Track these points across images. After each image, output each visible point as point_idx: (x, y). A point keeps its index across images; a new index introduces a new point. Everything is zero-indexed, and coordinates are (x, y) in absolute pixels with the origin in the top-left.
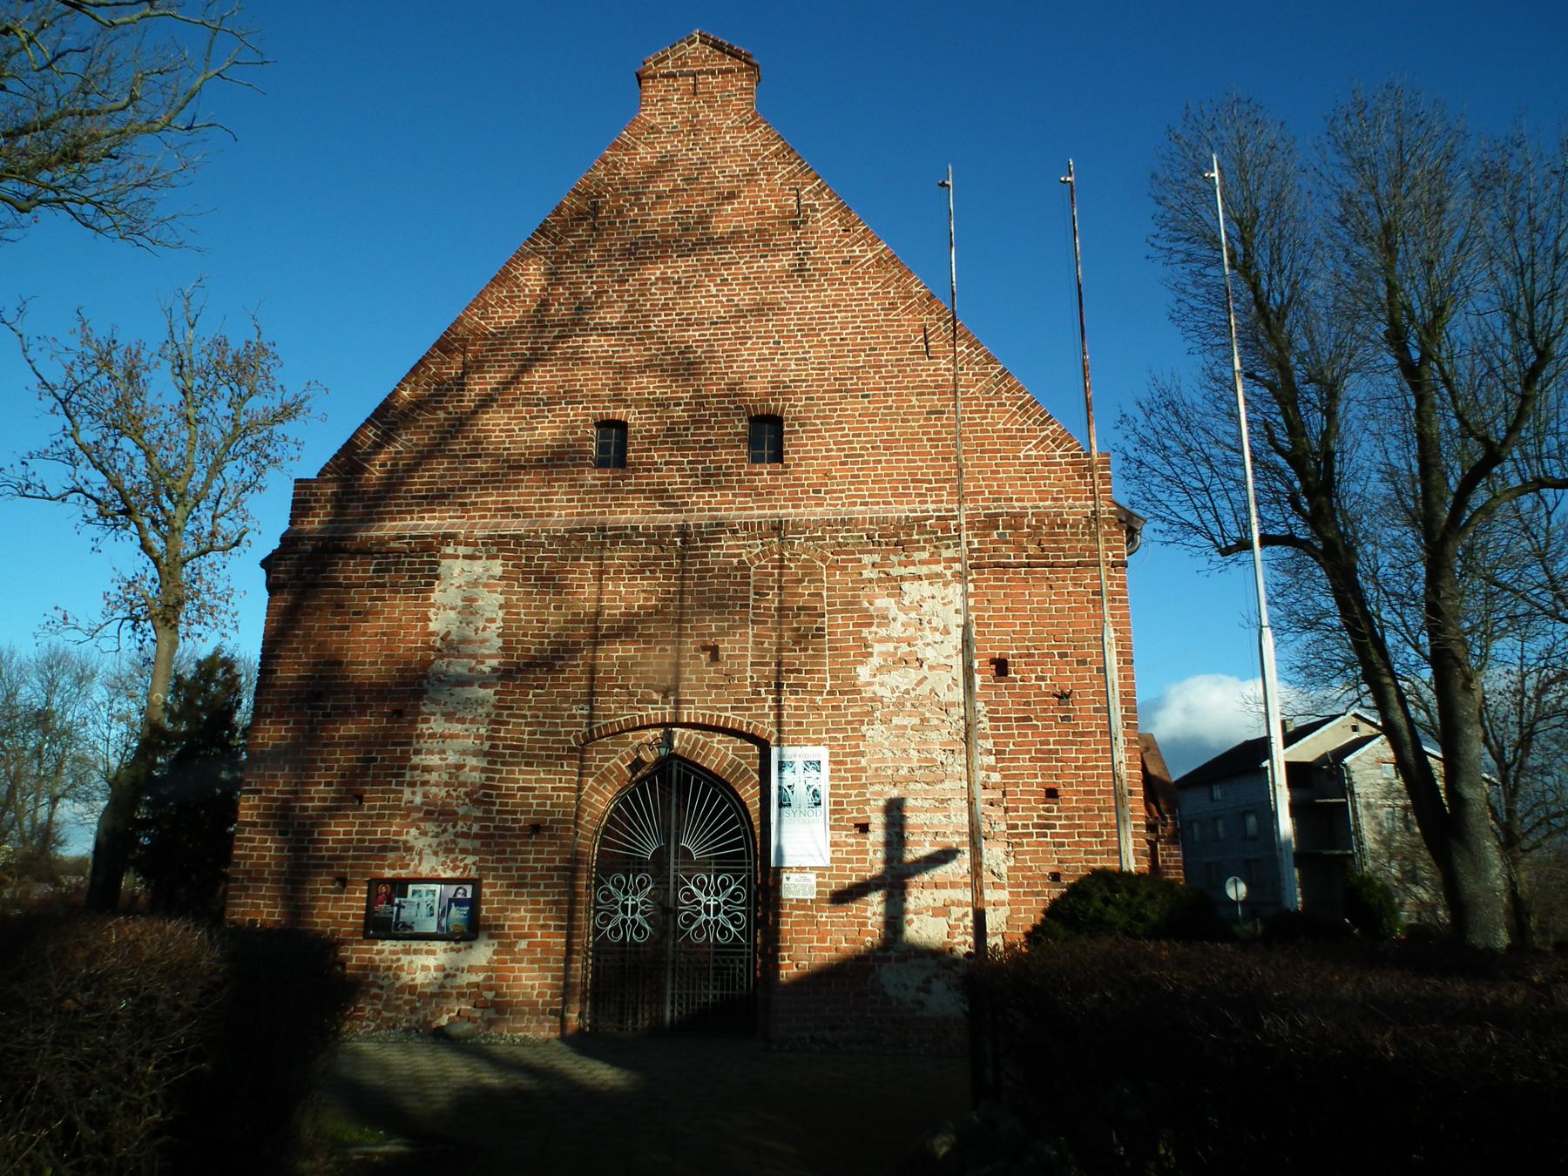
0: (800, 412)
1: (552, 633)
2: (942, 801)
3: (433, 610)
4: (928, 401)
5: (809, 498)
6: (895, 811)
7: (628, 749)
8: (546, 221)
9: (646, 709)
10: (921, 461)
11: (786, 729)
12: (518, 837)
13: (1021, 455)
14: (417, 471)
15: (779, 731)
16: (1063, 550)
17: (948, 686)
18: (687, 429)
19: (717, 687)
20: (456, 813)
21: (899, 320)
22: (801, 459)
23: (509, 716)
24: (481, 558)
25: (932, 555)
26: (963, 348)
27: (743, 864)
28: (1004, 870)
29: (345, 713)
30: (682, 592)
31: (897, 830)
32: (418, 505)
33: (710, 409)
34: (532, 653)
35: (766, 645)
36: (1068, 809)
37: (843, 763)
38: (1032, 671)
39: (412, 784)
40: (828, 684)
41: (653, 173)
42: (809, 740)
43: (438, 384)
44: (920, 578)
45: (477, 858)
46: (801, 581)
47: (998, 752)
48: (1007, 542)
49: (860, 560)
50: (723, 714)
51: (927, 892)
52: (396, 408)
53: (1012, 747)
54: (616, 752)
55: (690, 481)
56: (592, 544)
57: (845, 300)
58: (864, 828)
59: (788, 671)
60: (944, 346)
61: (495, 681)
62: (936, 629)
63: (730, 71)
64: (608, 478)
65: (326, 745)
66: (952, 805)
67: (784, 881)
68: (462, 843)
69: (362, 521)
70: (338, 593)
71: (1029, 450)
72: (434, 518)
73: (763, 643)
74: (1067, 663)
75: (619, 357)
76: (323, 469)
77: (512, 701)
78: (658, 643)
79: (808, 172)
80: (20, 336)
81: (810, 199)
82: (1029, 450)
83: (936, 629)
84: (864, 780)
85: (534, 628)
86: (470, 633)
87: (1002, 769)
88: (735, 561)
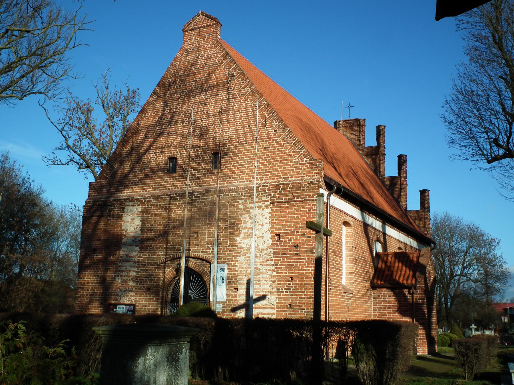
2: (259, 281)
5: (228, 181)
7: (175, 265)
8: (155, 89)
9: (177, 253)
10: (262, 165)
13: (293, 161)
16: (299, 196)
18: (193, 159)
19: (197, 245)
23: (142, 255)
24: (135, 206)
25: (259, 199)
26: (277, 123)
27: (205, 301)
28: (275, 303)
35: (211, 231)
36: (295, 284)
38: (288, 238)
40: (228, 244)
42: (222, 262)
45: (134, 298)
47: (276, 265)
48: (283, 194)
49: (238, 202)
54: (171, 266)
57: (241, 109)
60: (271, 123)
62: (259, 224)
63: (210, 25)
66: (262, 282)
71: (296, 159)
73: (210, 230)
74: (299, 235)
79: (232, 61)
80: (45, 110)
81: (232, 72)
82: (296, 159)
83: (259, 224)
84: (237, 275)
87: (276, 271)
88: (203, 203)
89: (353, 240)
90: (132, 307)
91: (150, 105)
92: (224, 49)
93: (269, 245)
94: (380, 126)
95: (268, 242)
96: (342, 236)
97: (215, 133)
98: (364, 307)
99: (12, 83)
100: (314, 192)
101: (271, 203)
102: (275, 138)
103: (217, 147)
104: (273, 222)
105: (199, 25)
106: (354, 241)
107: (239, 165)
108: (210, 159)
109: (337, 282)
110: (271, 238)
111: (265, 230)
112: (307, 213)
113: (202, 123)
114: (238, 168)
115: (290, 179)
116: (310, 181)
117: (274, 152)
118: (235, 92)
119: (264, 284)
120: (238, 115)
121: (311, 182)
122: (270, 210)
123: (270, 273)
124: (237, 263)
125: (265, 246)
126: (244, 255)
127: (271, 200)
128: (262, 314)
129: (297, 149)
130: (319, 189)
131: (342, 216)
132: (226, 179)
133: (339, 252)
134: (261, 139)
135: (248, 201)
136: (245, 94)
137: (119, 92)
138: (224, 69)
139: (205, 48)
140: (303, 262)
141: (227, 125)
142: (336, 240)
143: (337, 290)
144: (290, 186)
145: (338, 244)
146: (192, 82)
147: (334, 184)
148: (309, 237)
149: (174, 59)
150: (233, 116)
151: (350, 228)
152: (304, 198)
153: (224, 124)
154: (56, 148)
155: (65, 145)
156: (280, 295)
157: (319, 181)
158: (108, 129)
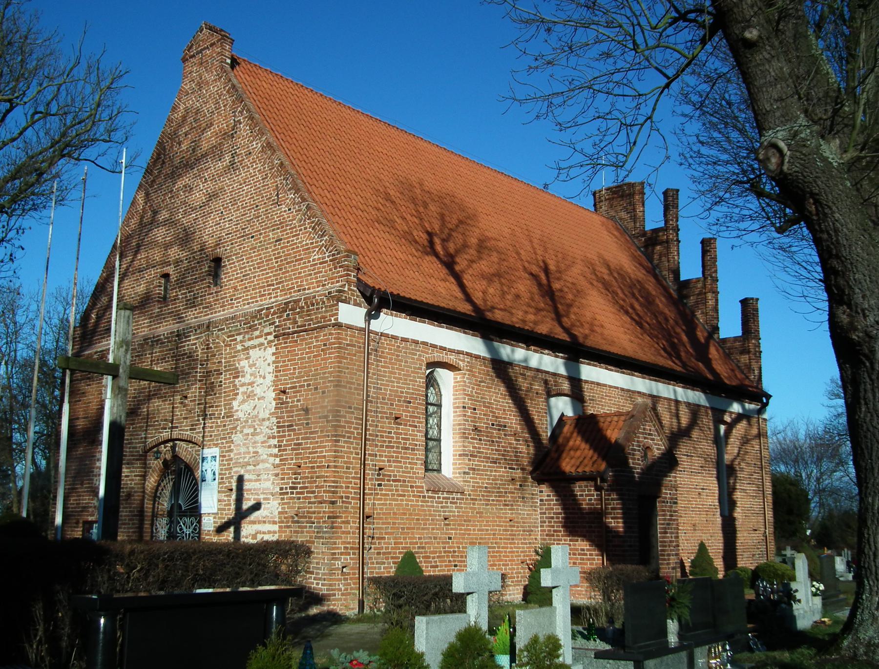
21: (268, 185)
41: (184, 118)
42: (214, 444)
47: (280, 446)
53: (285, 442)
58: (231, 490)
62: (260, 376)
66: (262, 477)
95: (270, 406)
101: (275, 337)
110: (274, 399)
112: (322, 350)
122: (273, 349)
123: (271, 459)
126: (241, 432)
127: (275, 331)
132: (227, 301)
138: (229, 114)
139: (207, 83)
140: (314, 438)
148: (324, 392)
151: (459, 374)
152: (319, 322)
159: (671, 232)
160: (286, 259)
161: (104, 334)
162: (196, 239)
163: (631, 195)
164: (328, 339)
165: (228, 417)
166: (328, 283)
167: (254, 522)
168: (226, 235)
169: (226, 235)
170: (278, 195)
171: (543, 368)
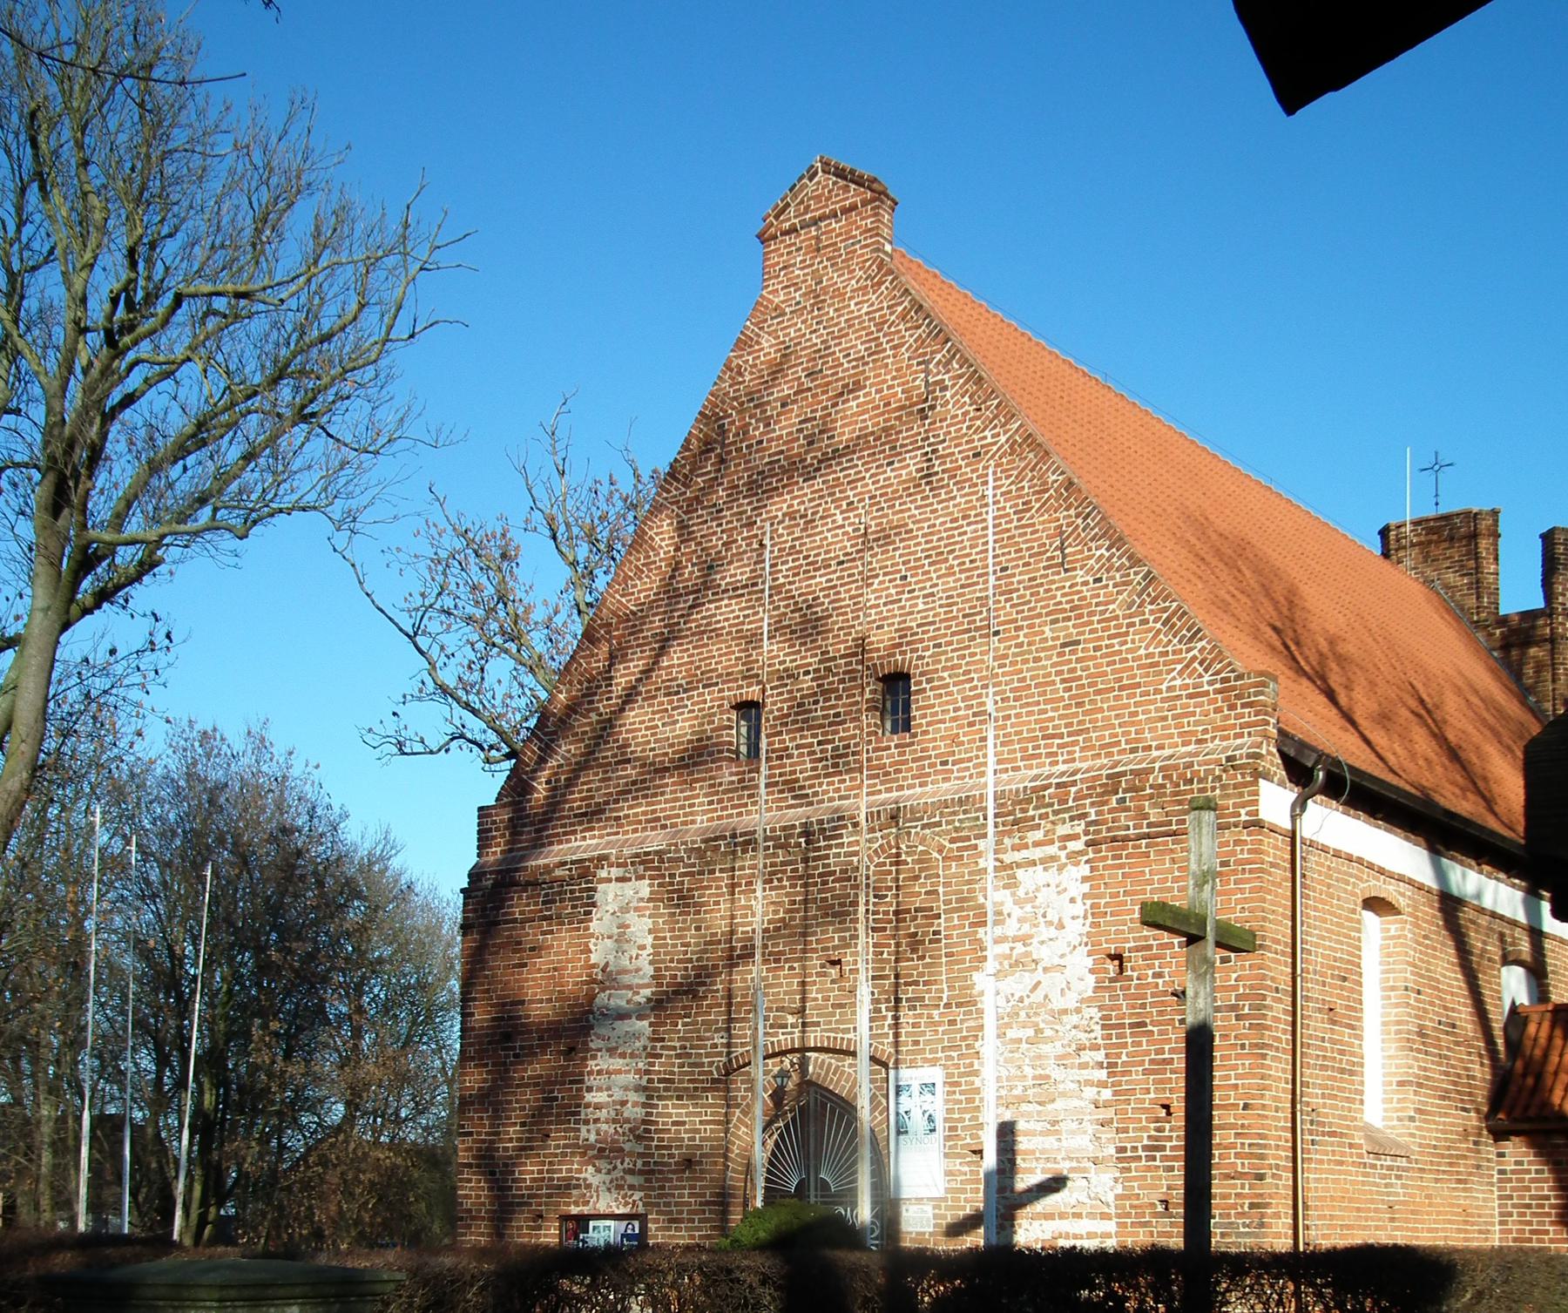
0: (928, 664)
1: (695, 957)
2: (1054, 1123)
3: (593, 940)
4: (1062, 629)
6: (1006, 1133)
9: (776, 1034)
10: (1053, 710)
11: (904, 1049)
12: (674, 1172)
13: (1164, 687)
14: (577, 785)
15: (897, 1052)
17: (1062, 990)
19: (841, 1006)
20: (622, 1150)
21: (1033, 525)
22: (929, 724)
23: (662, 1048)
24: (630, 879)
26: (1103, 551)
28: (1110, 1198)
29: (530, 1053)
30: (805, 901)
31: (1010, 1156)
32: (581, 823)
33: (838, 673)
34: (679, 980)
35: (885, 956)
37: (957, 1084)
38: (1151, 967)
39: (587, 1122)
40: (945, 996)
41: (777, 370)
42: (925, 1060)
43: (589, 681)
44: (1033, 863)
45: (642, 1194)
46: (917, 878)
47: (1110, 1065)
48: (1128, 809)
49: (975, 847)
50: (846, 1036)
51: (1036, 1223)
52: (554, 715)
53: (1124, 1058)
55: (820, 765)
56: (725, 854)
57: (975, 508)
59: (907, 984)
60: (1082, 552)
61: (648, 1012)
62: (1050, 923)
63: (853, 207)
64: (744, 772)
65: (518, 1086)
67: (904, 1214)
68: (630, 1179)
69: (535, 847)
70: (514, 928)
72: (593, 837)
73: (882, 953)
75: (749, 623)
76: (499, 793)
77: (665, 1032)
78: (787, 961)
80: (353, 565)
81: (938, 374)
83: (1050, 923)
85: (678, 953)
86: (625, 962)
89: (1408, 963)
90: (636, 1224)
91: (661, 520)
92: (906, 290)
93: (1085, 995)
94: (1552, 532)
95: (1080, 986)
96: (1359, 949)
97: (885, 604)
98: (1459, 1206)
99: (224, 478)
100: (1241, 795)
101: (1088, 844)
102: (1097, 604)
103: (894, 655)
104: (1096, 912)
105: (817, 209)
106: (1415, 966)
107: (975, 715)
108: (872, 700)
109: (1341, 1117)
110: (1092, 971)
111: (1069, 944)
113: (842, 570)
114: (971, 724)
115: (1155, 753)
116: (1223, 756)
117: (1095, 658)
118: (950, 447)
119: (1073, 1132)
120: (965, 533)
121: (1229, 759)
122: (1085, 870)
123: (1090, 1092)
124: (976, 1061)
125: (1071, 1001)
127: (1086, 833)
128: (1067, 1236)
129: (1175, 641)
130: (1255, 783)
131: (1361, 879)
132: (932, 765)
133: (1348, 1008)
134: (1047, 614)
135: (1007, 841)
136: (986, 453)
137: (606, 481)
141: (929, 572)
142: (1333, 968)
143: (1341, 1145)
144: (1156, 778)
145: (1345, 979)
146: (800, 423)
147: (1316, 763)
149: (736, 345)
150: (949, 537)
151: (1396, 922)
153: (916, 568)
154: (404, 697)
155: (431, 686)
156: (1129, 1170)
157: (1258, 756)
158: (575, 617)
159: (1560, 619)
160: (1090, 685)
161: (572, 824)
162: (832, 630)
163: (1474, 536)
164: (1233, 853)
165: (959, 1005)
166: (1214, 738)
167: (1049, 1216)
168: (919, 626)
169: (919, 626)
170: (1062, 548)
171: (1500, 911)
